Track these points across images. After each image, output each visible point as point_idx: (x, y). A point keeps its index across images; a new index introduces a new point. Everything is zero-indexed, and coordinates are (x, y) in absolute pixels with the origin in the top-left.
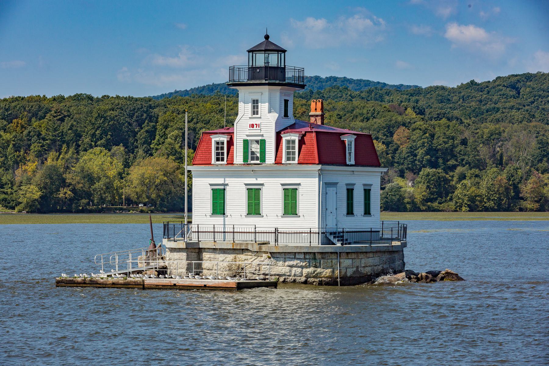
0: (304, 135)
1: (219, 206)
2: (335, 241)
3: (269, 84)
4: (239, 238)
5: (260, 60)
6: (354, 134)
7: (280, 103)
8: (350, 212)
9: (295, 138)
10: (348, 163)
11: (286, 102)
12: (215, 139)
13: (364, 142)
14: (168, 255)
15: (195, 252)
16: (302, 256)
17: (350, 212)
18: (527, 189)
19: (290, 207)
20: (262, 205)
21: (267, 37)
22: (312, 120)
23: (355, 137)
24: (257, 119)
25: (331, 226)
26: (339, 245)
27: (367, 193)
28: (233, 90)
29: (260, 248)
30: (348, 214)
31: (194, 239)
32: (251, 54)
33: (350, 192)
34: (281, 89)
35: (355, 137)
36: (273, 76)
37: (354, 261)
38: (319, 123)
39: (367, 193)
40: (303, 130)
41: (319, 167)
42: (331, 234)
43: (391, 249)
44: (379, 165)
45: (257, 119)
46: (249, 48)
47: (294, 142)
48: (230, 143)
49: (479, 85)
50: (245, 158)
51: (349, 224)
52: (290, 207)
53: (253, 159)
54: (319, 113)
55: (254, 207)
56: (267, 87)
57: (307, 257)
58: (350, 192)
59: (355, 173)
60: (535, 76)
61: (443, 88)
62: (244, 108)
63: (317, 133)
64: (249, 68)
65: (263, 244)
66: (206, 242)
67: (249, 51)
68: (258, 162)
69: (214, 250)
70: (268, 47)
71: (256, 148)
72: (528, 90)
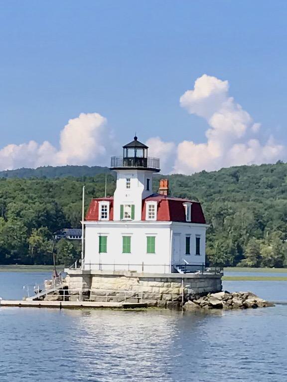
0: (160, 202)
1: (102, 248)
2: (179, 270)
3: (138, 169)
4: (118, 268)
5: (131, 153)
6: (191, 202)
7: (145, 181)
8: (188, 252)
9: (155, 203)
10: (187, 220)
11: (148, 180)
12: (101, 203)
13: (196, 207)
14: (68, 278)
15: (88, 277)
16: (160, 280)
17: (188, 252)
18: (247, 250)
19: (151, 249)
20: (130, 246)
21: (136, 138)
22: (161, 192)
23: (192, 204)
24: (129, 191)
25: (177, 262)
26: (182, 273)
27: (198, 240)
28: (115, 172)
29: (132, 275)
30: (197, 254)
31: (87, 268)
32: (125, 149)
33: (188, 239)
34: (145, 172)
35: (192, 204)
36: (140, 164)
37: (192, 284)
38: (166, 194)
39: (198, 240)
40: (160, 198)
41: (171, 223)
42: (177, 266)
43: (215, 277)
44: (204, 222)
45: (129, 191)
46: (124, 145)
47: (153, 206)
48: (111, 206)
49: (208, 173)
50: (122, 217)
51: (186, 261)
52: (151, 249)
53: (126, 217)
54: (166, 188)
55: (127, 249)
56: (136, 171)
57: (163, 280)
58: (188, 239)
59: (192, 227)
60: (250, 167)
61: (181, 175)
62: (121, 183)
63: (169, 200)
64: (124, 158)
65: (134, 272)
66: (95, 270)
67: (124, 147)
68: (130, 219)
69: (101, 276)
70: (136, 145)
71: (128, 210)
72: (245, 178)
